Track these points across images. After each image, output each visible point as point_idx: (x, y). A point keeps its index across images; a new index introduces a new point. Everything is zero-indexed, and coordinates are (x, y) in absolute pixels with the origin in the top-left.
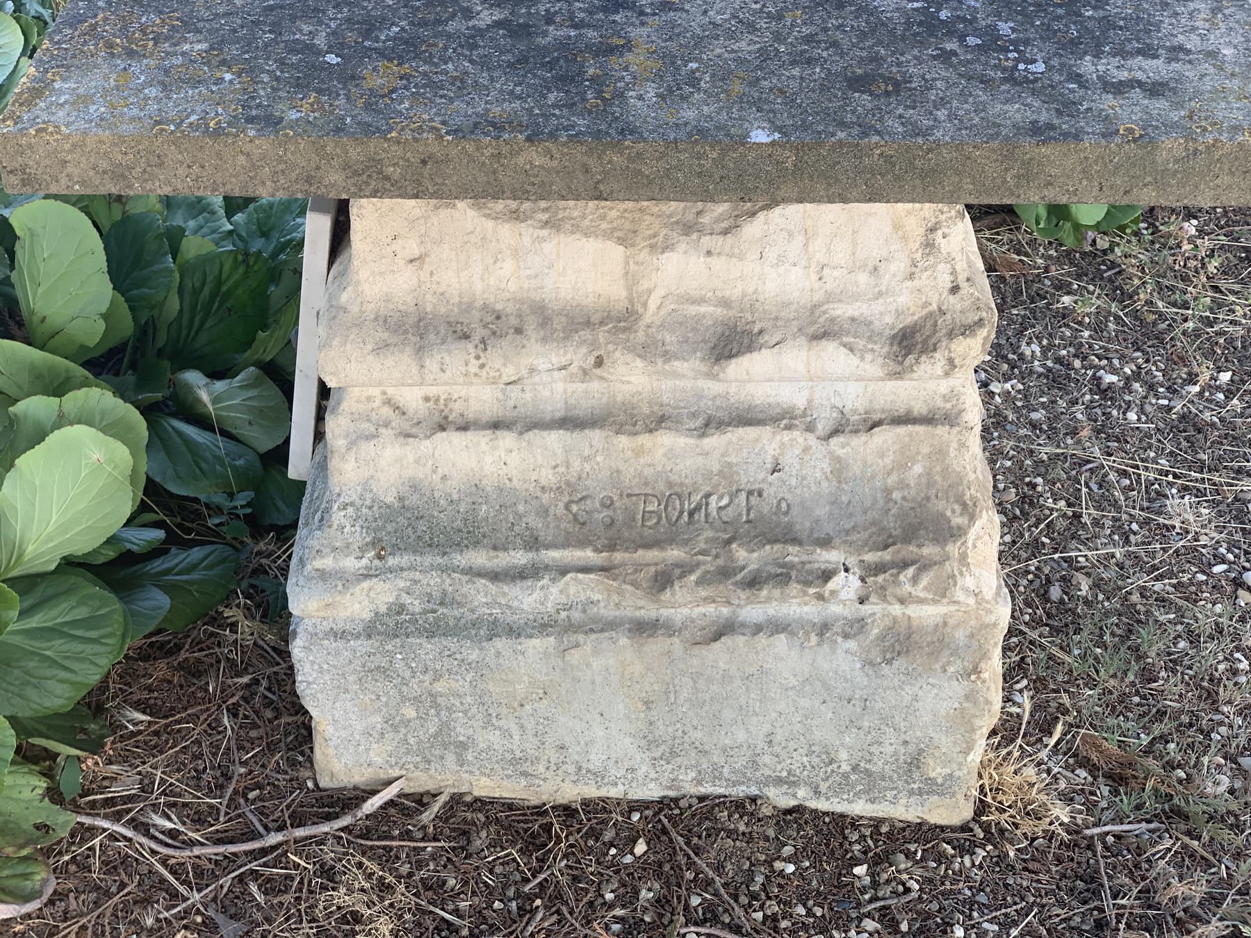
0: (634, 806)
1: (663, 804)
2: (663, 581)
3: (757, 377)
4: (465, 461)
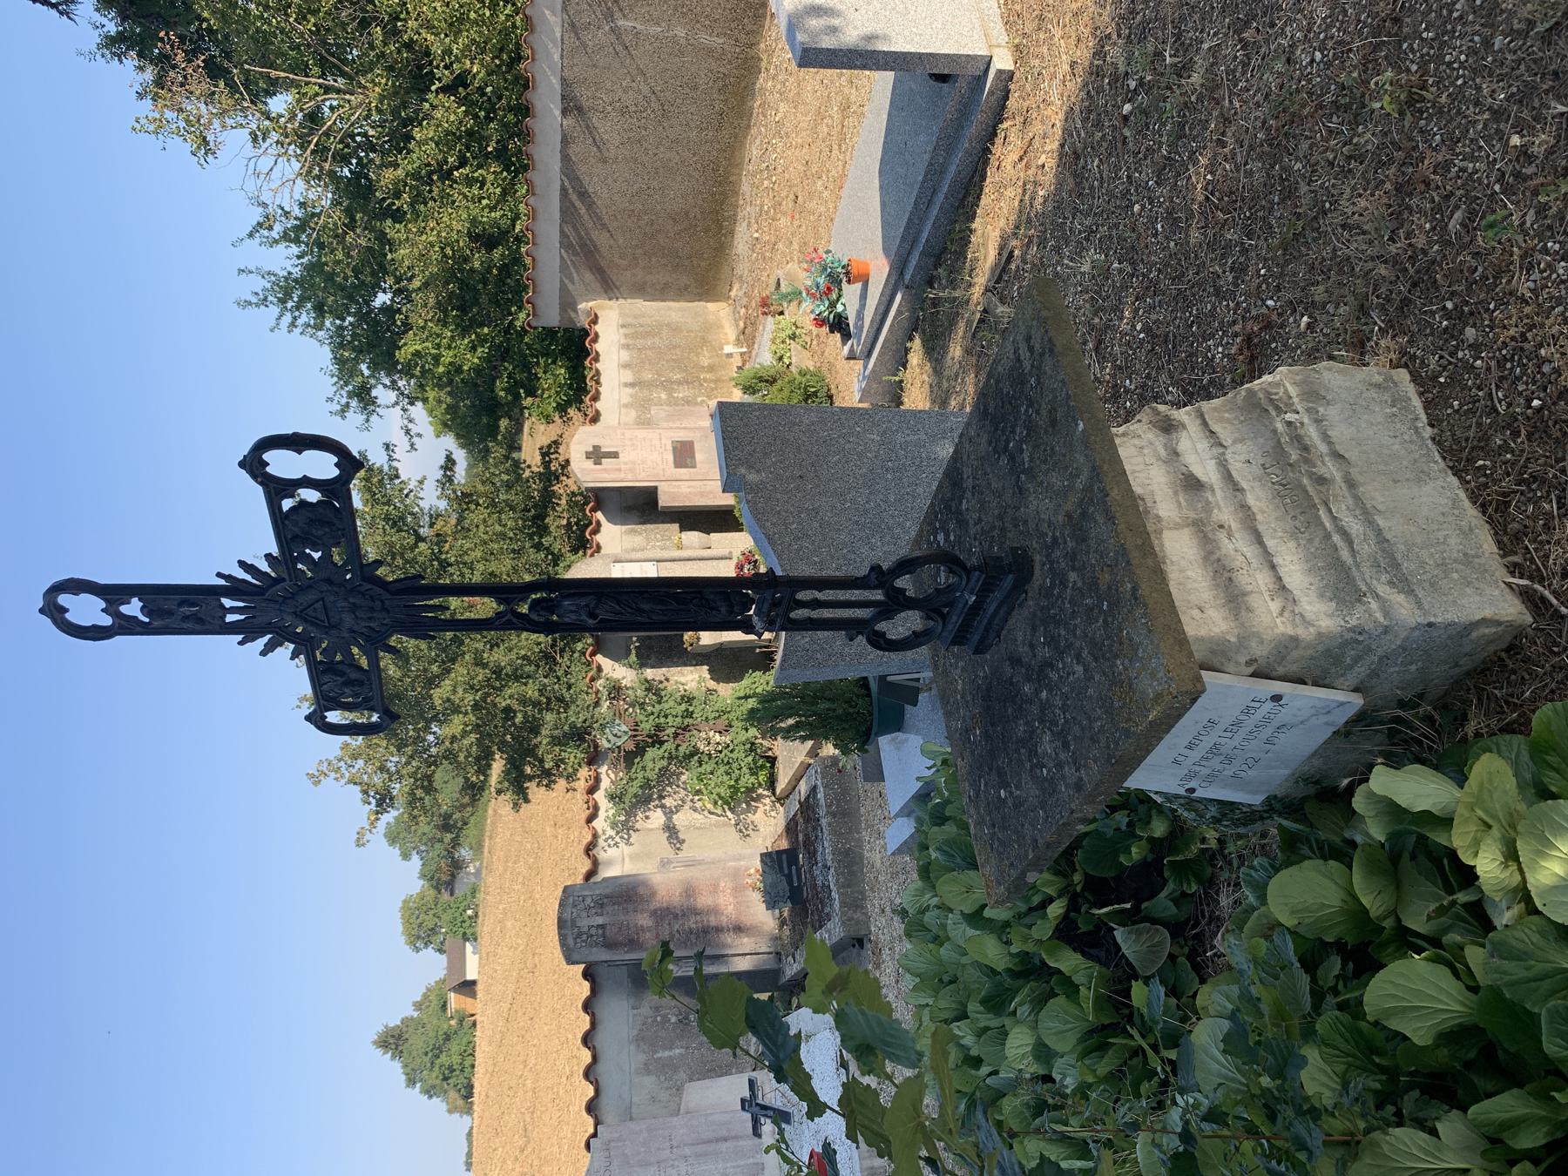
0: (1464, 482)
1: (1457, 473)
2: (1321, 480)
3: (1206, 470)
4: (1295, 573)
